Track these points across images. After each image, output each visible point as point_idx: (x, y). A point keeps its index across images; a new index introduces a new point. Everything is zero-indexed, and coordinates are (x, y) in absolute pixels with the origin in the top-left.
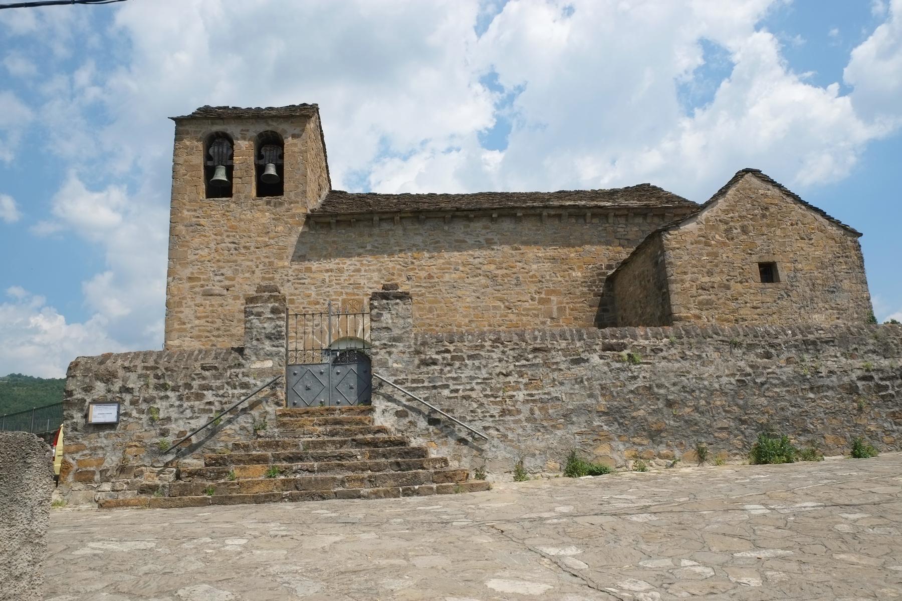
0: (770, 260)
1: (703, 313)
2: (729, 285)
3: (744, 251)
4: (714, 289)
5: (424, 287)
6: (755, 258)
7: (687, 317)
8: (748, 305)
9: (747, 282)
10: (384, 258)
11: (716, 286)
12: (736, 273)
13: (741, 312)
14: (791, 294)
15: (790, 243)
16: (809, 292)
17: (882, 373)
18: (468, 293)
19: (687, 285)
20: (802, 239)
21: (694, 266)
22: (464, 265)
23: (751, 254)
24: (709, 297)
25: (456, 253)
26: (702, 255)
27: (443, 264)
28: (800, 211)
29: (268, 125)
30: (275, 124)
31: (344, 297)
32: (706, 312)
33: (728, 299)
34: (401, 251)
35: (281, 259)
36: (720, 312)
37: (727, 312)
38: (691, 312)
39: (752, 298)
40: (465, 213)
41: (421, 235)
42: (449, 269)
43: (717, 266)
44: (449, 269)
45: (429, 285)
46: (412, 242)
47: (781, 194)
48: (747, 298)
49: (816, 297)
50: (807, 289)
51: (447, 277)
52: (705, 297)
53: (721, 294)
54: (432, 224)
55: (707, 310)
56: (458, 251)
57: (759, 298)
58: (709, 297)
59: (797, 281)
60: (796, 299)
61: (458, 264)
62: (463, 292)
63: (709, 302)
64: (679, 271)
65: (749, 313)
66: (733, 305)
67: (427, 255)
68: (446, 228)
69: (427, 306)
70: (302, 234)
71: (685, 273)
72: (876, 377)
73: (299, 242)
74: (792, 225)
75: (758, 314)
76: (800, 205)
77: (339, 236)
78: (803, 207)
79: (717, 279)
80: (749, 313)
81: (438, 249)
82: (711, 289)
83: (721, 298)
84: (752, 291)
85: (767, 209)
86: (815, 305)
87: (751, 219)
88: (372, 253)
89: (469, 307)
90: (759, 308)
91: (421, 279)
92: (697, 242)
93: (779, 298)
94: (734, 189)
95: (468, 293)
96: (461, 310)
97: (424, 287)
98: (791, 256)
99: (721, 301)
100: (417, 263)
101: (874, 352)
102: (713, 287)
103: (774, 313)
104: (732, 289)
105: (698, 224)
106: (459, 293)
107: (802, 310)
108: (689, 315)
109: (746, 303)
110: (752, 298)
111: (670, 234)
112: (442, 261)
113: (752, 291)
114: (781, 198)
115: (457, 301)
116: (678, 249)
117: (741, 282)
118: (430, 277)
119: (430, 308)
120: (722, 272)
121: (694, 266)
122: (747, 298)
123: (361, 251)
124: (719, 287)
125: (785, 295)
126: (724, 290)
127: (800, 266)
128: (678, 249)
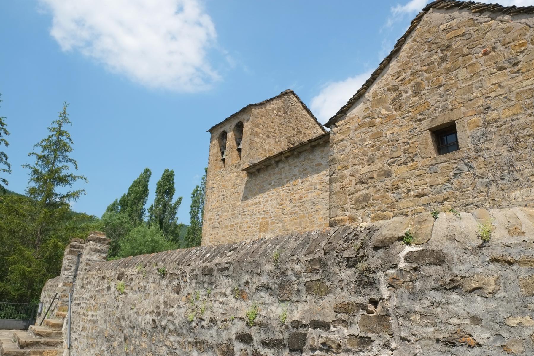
0: (447, 120)
1: (359, 213)
2: (390, 171)
3: (412, 119)
4: (373, 180)
5: (297, 206)
6: (426, 124)
7: (342, 221)
8: (412, 193)
9: (413, 160)
10: (279, 189)
11: (375, 175)
12: (401, 153)
13: (401, 205)
14: (474, 165)
15: (479, 84)
16: (505, 154)
17: (266, 332)
18: (322, 206)
19: (347, 181)
20: (501, 69)
21: (356, 156)
22: (320, 184)
23: (420, 120)
24: (367, 192)
25: (316, 175)
26: (364, 140)
27: (308, 186)
28: (501, 25)
29: (238, 118)
30: (240, 117)
31: (261, 221)
32: (362, 210)
33: (387, 190)
34: (287, 181)
35: (238, 201)
36: (377, 208)
37: (384, 207)
38: (347, 214)
39: (418, 182)
40: (317, 141)
41: (297, 166)
42: (311, 189)
43: (378, 149)
44: (311, 189)
45: (300, 204)
46: (293, 173)
47: (471, 16)
48: (411, 183)
49: (519, 160)
50: (503, 151)
51: (310, 196)
52: (363, 192)
53: (380, 184)
54: (303, 156)
55: (363, 208)
56: (317, 173)
57: (428, 180)
58: (367, 192)
59: (486, 140)
60: (481, 171)
61: (316, 184)
62: (319, 206)
63: (365, 198)
64: (340, 167)
65: (411, 204)
66: (392, 196)
67: (300, 181)
68: (311, 157)
69: (299, 220)
70: (247, 181)
71: (346, 167)
72: (256, 338)
73: (246, 188)
74: (485, 54)
75: (423, 205)
76: (500, 18)
77: (263, 177)
78: (507, 17)
79: (378, 165)
80: (411, 204)
81: (306, 175)
82: (369, 181)
83: (379, 190)
84: (418, 172)
85: (448, 47)
86: (517, 175)
87: (426, 71)
88: (275, 186)
89: (322, 218)
90: (425, 195)
91: (296, 200)
92: (361, 126)
93: (455, 175)
94: (411, 40)
95: (322, 206)
96: (317, 221)
97: (297, 206)
98: (480, 102)
99: (379, 194)
100: (295, 188)
101: (268, 289)
102: (372, 178)
103: (446, 199)
104: (393, 176)
105: (365, 103)
106: (316, 207)
107: (493, 189)
108: (345, 217)
109: (409, 191)
110: (418, 182)
111: (337, 127)
112: (308, 183)
113: (418, 172)
114: (471, 21)
115: (315, 214)
116: (342, 140)
117: (405, 163)
118: (301, 198)
119: (300, 222)
120: (384, 155)
121: (356, 156)
122: (411, 183)
123: (269, 187)
124: (378, 176)
125: (466, 168)
126: (383, 178)
127: (493, 115)
128: (342, 140)
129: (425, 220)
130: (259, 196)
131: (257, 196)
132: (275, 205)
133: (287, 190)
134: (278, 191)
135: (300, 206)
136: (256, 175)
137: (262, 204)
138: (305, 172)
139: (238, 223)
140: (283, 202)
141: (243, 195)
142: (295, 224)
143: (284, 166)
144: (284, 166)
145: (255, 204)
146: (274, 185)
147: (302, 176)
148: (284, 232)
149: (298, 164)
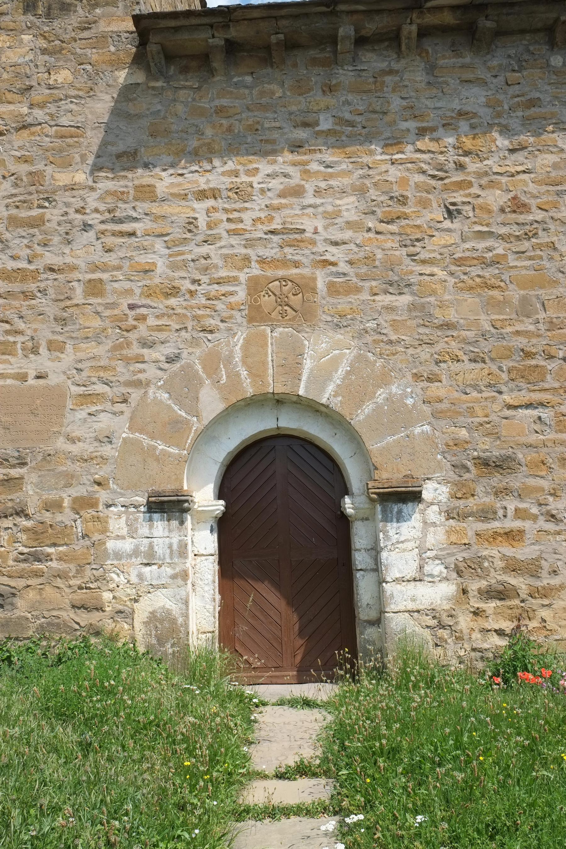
5: (501, 237)
10: (371, 153)
31: (256, 270)
73: (116, 112)
97: (501, 237)
100: (472, 166)
123: (301, 134)
129: (52, 270)
130: (230, 165)
131: (217, 162)
132: (351, 216)
133: (425, 167)
134: (366, 159)
135: (518, 238)
136: (113, 551)
137: (260, 202)
138: (528, 113)
139: (73, 268)
140: (407, 210)
141: (104, 144)
142: (500, 305)
143: (395, 66)
144: (395, 66)
145: (202, 195)
146: (329, 133)
147: (515, 123)
148: (421, 330)
149: (481, 73)
